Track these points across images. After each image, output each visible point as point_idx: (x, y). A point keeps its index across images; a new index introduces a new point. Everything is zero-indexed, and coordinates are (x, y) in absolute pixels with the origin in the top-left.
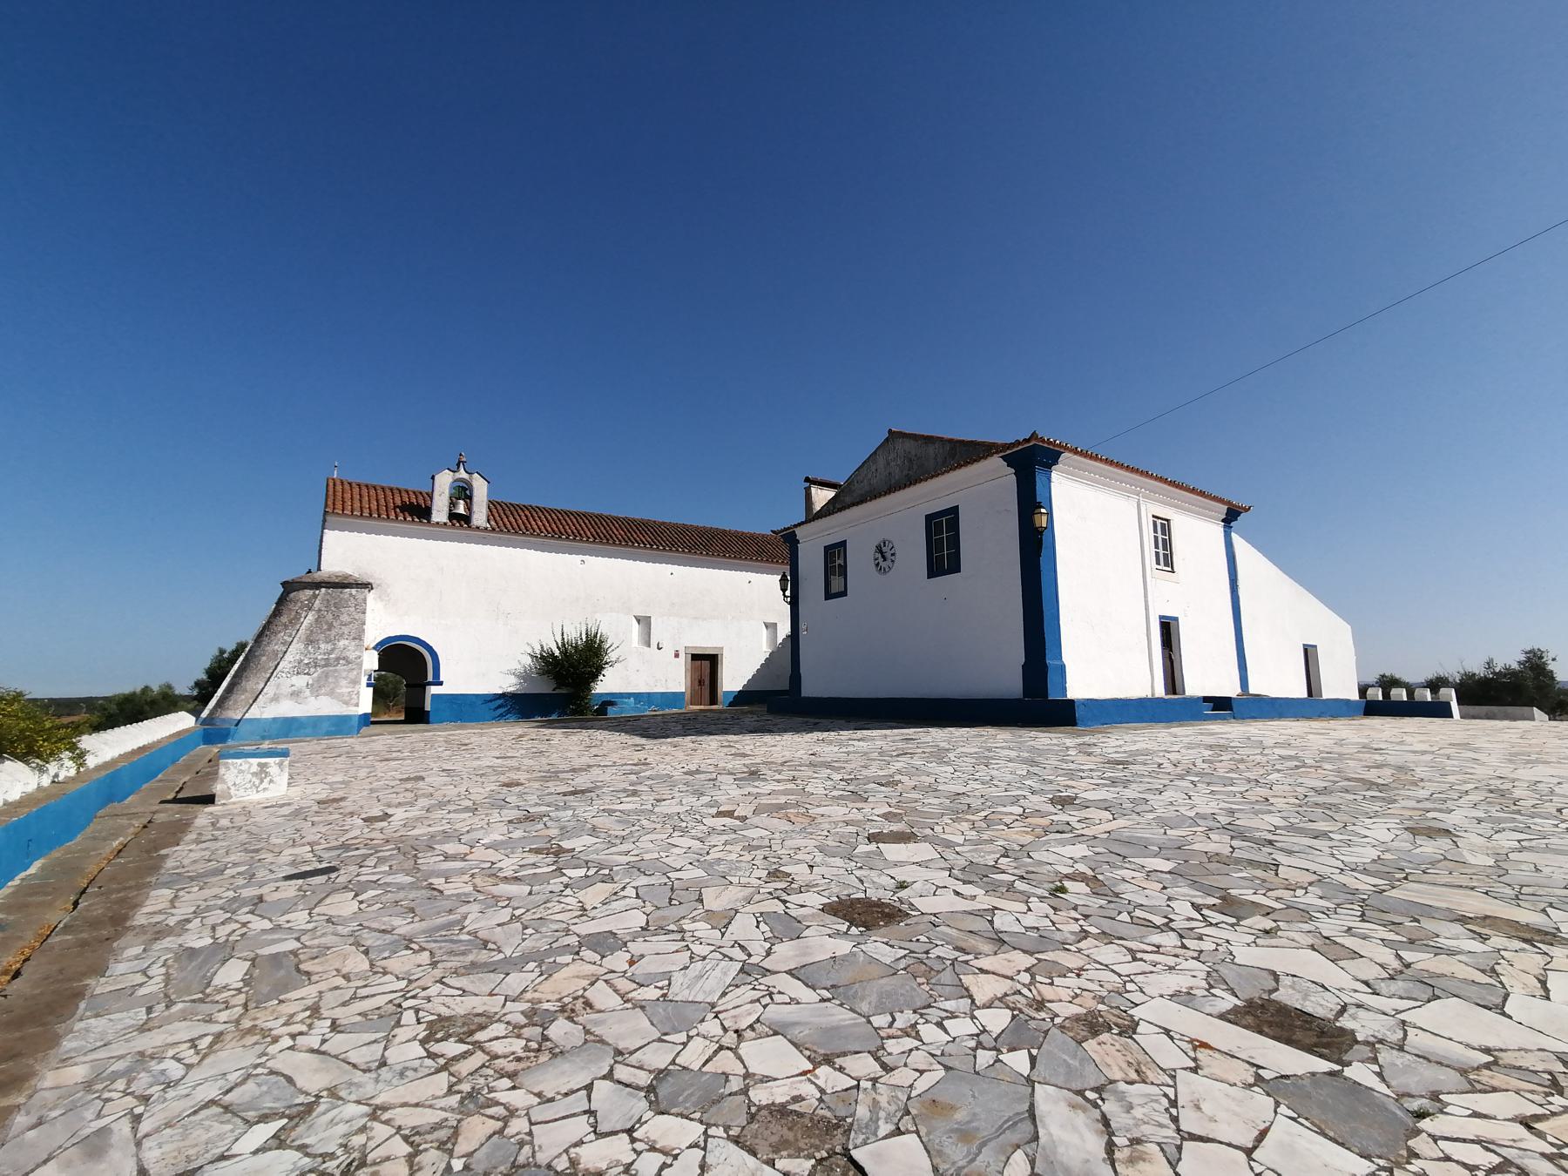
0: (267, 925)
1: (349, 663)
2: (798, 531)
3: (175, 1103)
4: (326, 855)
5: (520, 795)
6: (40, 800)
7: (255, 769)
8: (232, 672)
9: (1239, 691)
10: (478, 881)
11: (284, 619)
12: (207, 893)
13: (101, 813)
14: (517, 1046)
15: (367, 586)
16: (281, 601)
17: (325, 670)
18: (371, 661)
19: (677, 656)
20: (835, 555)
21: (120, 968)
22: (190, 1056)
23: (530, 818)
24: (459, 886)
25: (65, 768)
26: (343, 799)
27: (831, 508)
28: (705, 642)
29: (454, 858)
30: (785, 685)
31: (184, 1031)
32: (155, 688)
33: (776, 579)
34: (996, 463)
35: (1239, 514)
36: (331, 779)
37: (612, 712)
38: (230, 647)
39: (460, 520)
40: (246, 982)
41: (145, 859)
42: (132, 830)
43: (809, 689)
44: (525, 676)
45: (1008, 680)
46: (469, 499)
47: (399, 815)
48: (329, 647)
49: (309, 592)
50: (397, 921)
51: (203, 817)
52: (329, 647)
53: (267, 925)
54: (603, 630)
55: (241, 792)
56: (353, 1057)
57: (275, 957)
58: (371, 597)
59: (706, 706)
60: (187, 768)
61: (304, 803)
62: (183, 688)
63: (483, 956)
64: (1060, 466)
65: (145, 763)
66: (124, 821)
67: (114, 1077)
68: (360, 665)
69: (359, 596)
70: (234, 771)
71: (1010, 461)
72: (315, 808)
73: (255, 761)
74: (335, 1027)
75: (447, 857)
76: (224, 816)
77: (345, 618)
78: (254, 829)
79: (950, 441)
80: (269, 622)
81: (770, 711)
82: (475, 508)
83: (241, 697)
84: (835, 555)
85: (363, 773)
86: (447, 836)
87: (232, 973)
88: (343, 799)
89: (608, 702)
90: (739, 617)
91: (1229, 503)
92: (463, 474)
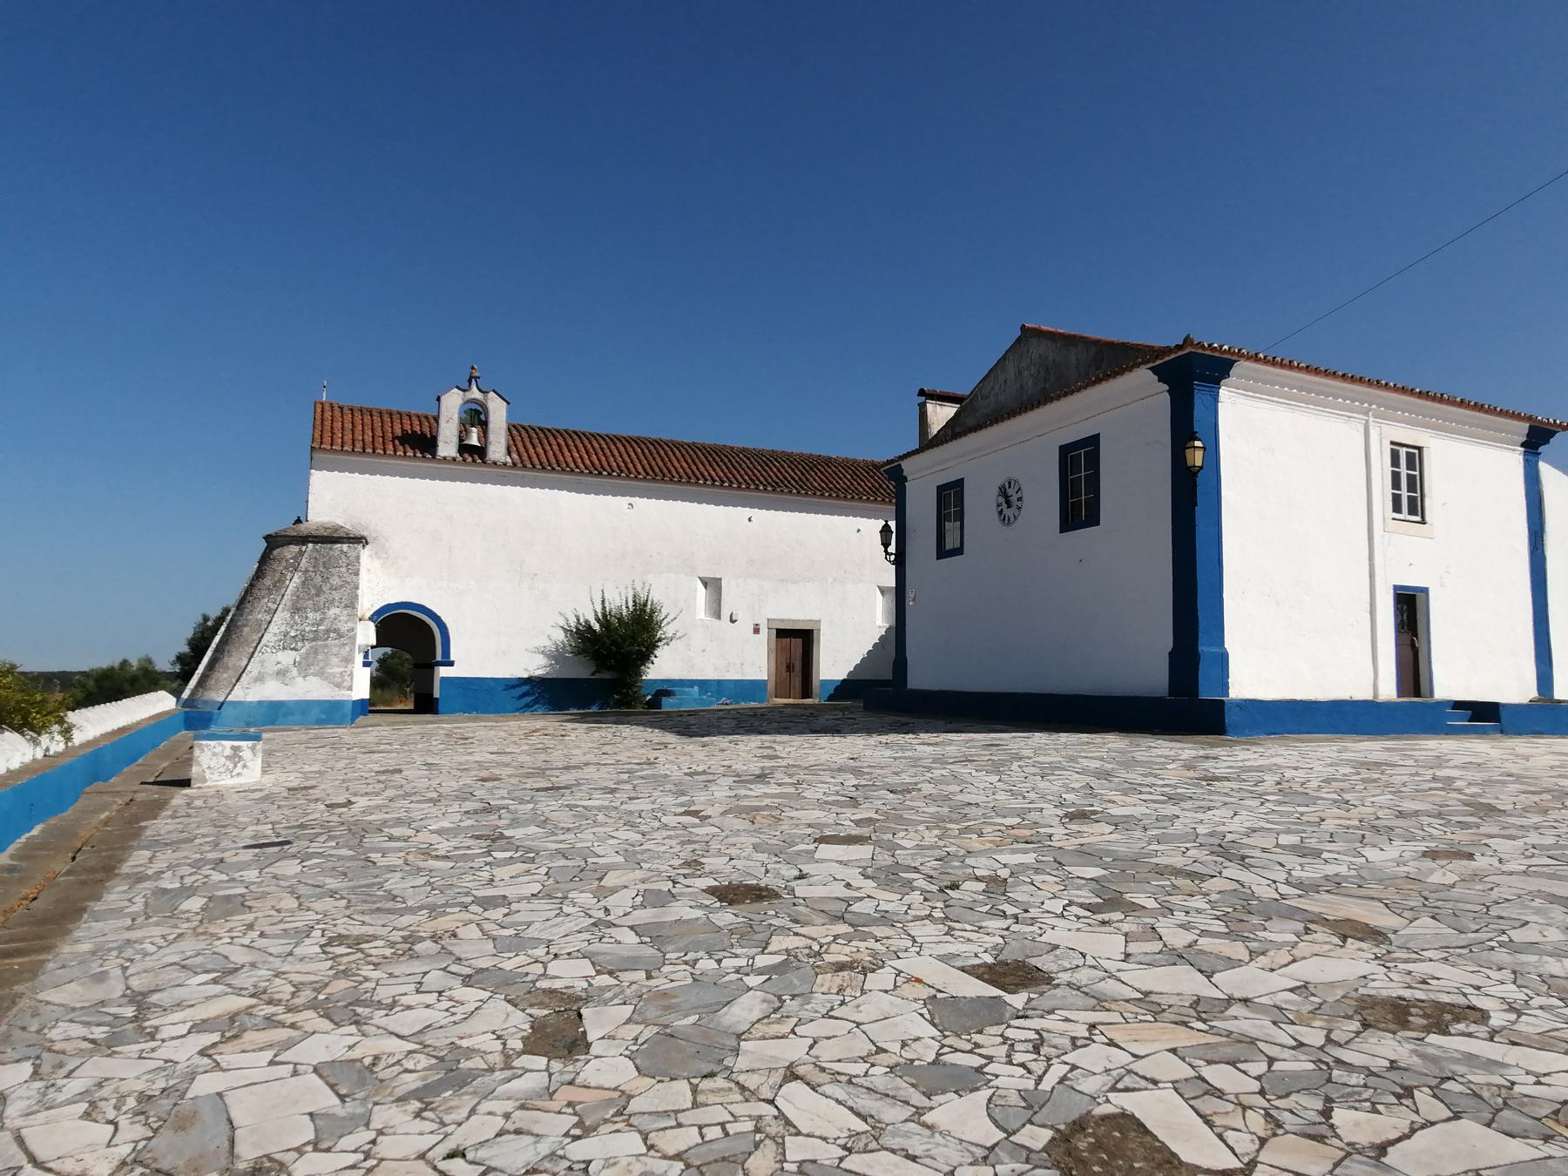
0: (224, 877)
1: (340, 636)
2: (905, 464)
3: (149, 962)
4: (283, 832)
5: (490, 790)
6: (35, 771)
7: (228, 752)
8: (213, 645)
9: (1534, 694)
10: (411, 858)
11: (268, 582)
12: (179, 854)
13: (87, 789)
14: (388, 952)
15: (360, 540)
16: (265, 559)
17: (315, 644)
18: (367, 634)
19: (756, 631)
20: (950, 497)
21: (113, 897)
22: (161, 942)
23: (488, 809)
24: (394, 860)
25: (53, 743)
26: (312, 787)
27: (953, 430)
28: (795, 613)
29: (398, 839)
30: (887, 674)
31: (157, 931)
32: (135, 663)
33: (871, 527)
34: (1143, 377)
35: (1552, 434)
36: (307, 768)
37: (668, 704)
38: (214, 613)
39: (473, 454)
40: (202, 909)
41: (129, 828)
42: (115, 807)
43: (918, 679)
44: (556, 656)
45: (1149, 673)
46: (484, 425)
47: (362, 802)
48: (318, 616)
49: (294, 549)
50: (328, 880)
51: (179, 797)
52: (318, 616)
53: (224, 877)
54: (656, 596)
55: (216, 776)
56: (271, 950)
57: (228, 898)
58: (365, 554)
59: (796, 695)
60: (166, 755)
61: (276, 790)
62: (164, 663)
63: (390, 905)
64: (1232, 379)
65: (127, 743)
66: (107, 798)
67: (110, 950)
68: (353, 638)
69: (352, 554)
70: (208, 753)
71: (1162, 373)
72: (285, 794)
73: (228, 744)
74: (262, 935)
75: (391, 838)
76: (198, 798)
77: (335, 581)
78: (224, 810)
79: (1097, 342)
80: (252, 585)
81: (868, 708)
82: (492, 437)
83: (222, 676)
84: (950, 497)
85: (341, 764)
86: (399, 822)
87: (195, 904)
88: (312, 787)
89: (665, 690)
90: (833, 578)
91: (1530, 418)
92: (475, 393)
